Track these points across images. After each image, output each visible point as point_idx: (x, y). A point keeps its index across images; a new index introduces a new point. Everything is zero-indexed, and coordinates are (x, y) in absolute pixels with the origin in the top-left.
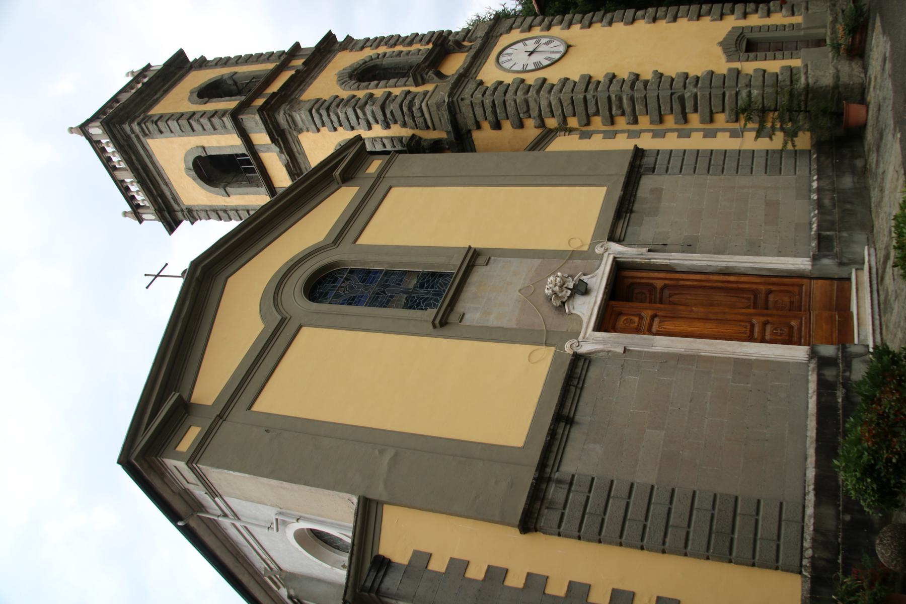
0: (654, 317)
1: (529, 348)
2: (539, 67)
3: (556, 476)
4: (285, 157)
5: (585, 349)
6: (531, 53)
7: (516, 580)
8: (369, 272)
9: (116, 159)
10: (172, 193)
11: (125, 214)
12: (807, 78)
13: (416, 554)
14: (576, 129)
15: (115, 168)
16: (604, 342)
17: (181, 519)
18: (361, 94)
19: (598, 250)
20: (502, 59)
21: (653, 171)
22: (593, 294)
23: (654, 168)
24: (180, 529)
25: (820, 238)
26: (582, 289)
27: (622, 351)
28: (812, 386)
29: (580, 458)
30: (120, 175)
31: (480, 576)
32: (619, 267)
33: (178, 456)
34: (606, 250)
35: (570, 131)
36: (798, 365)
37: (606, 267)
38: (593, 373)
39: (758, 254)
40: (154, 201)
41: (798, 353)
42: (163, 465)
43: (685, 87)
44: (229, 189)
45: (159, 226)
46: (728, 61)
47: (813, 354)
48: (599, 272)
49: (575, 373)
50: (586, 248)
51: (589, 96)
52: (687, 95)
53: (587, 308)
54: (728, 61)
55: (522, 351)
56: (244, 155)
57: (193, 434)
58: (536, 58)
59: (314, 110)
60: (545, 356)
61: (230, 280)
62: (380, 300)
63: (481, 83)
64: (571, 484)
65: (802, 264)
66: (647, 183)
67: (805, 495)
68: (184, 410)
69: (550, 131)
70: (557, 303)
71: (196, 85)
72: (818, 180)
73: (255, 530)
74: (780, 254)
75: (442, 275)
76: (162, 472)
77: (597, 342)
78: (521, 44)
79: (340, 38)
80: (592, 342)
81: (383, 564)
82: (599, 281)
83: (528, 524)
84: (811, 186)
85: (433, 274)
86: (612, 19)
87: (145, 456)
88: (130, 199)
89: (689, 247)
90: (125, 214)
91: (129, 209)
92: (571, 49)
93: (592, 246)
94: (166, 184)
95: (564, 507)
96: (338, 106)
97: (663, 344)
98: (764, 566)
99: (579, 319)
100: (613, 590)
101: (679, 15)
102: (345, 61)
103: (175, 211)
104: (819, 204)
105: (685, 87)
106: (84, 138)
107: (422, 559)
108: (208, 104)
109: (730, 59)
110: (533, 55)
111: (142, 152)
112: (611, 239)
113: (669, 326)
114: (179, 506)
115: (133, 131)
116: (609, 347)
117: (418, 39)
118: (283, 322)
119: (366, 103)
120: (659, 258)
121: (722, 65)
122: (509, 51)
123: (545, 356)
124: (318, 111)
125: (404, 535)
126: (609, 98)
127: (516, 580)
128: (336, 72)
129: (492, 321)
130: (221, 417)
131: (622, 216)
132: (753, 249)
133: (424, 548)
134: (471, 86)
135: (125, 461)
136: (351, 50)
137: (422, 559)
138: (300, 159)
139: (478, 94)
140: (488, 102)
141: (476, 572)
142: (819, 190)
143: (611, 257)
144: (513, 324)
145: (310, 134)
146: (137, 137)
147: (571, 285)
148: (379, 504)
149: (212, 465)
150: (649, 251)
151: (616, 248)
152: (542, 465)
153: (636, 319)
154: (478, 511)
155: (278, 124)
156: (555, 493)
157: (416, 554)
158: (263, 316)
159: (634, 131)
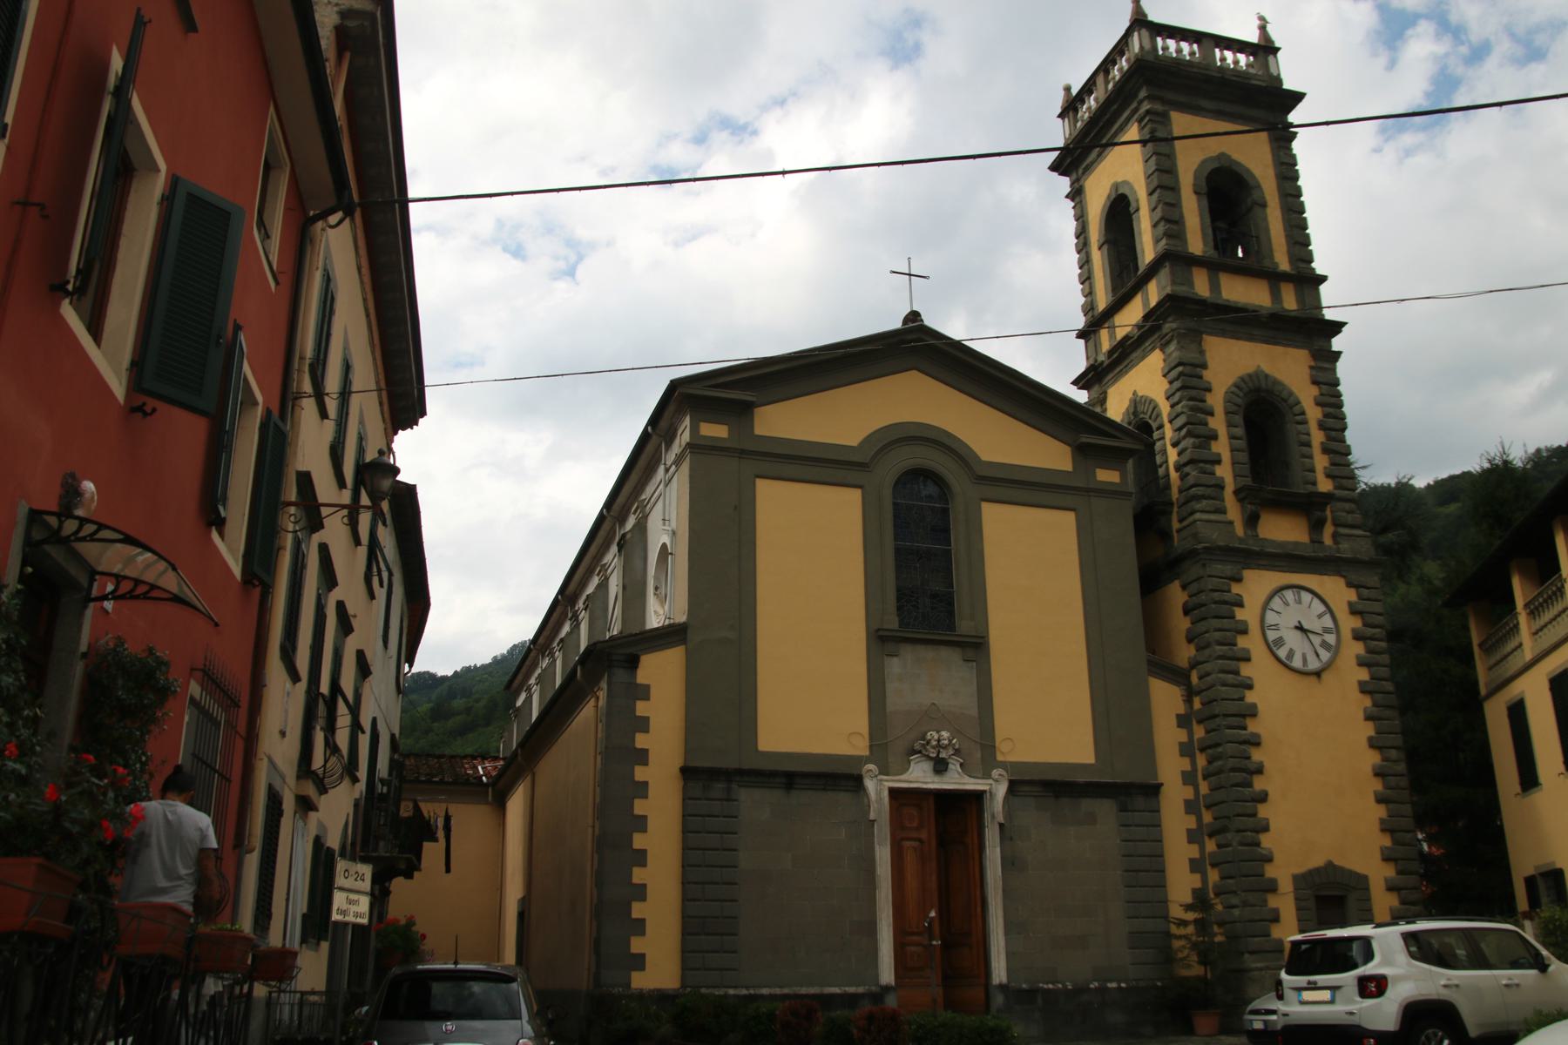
0: (920, 840)
1: (865, 730)
2: (1271, 648)
3: (734, 786)
5: (870, 784)
6: (1300, 628)
7: (640, 773)
8: (947, 531)
9: (1116, 73)
10: (1092, 163)
11: (1068, 89)
12: (1261, 969)
13: (647, 687)
14: (1191, 707)
15: (1107, 72)
16: (880, 799)
18: (1218, 423)
19: (995, 773)
20: (1289, 595)
22: (936, 779)
23: (1126, 810)
24: (645, 432)
26: (940, 767)
27: (872, 817)
28: (852, 990)
29: (755, 805)
30: (1100, 80)
32: (977, 797)
35: (1188, 700)
36: (877, 976)
37: (971, 784)
38: (843, 797)
39: (1007, 933)
41: (887, 975)
42: (684, 415)
43: (1238, 831)
48: (967, 779)
49: (840, 779)
50: (1000, 758)
52: (1229, 836)
53: (919, 776)
55: (862, 724)
57: (716, 431)
58: (1293, 640)
59: (1180, 368)
60: (860, 747)
61: (914, 372)
64: (728, 800)
65: (999, 972)
66: (1105, 809)
67: (747, 988)
68: (740, 412)
69: (1188, 677)
70: (917, 747)
72: (1120, 988)
73: (660, 503)
74: (1010, 955)
75: (951, 614)
76: (680, 413)
77: (878, 793)
78: (1322, 608)
79: (1337, 343)
80: (876, 787)
81: (633, 663)
82: (956, 780)
83: (687, 772)
84: (1111, 981)
85: (951, 604)
86: (1379, 719)
87: (687, 398)
88: (1088, 88)
90: (1068, 89)
93: (1004, 765)
96: (1191, 399)
97: (883, 855)
98: (684, 960)
99: (905, 768)
101: (1391, 806)
104: (1080, 990)
105: (1238, 831)
106: (1127, 24)
107: (644, 693)
108: (1194, 197)
109: (1301, 881)
110: (1298, 633)
112: (1012, 784)
113: (910, 859)
114: (663, 424)
115: (1141, 102)
116: (874, 806)
117: (1338, 459)
118: (862, 466)
119: (1197, 436)
120: (992, 837)
121: (1282, 871)
122: (1306, 597)
123: (860, 747)
124: (1181, 374)
125: (662, 672)
127: (640, 773)
128: (1266, 369)
129: (891, 687)
130: (743, 453)
131: (1047, 788)
133: (653, 691)
134: (1228, 569)
135: (674, 386)
136: (1311, 368)
137: (644, 693)
139: (1212, 583)
140: (1203, 597)
141: (641, 741)
142: (1103, 990)
143: (986, 788)
144: (890, 708)
145: (1161, 364)
146: (1136, 110)
148: (683, 641)
149: (691, 469)
150: (1001, 825)
152: (741, 772)
154: (693, 728)
156: (719, 788)
157: (647, 687)
158: (868, 440)
159: (1196, 776)
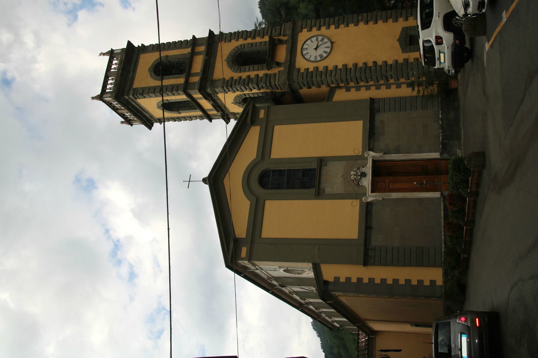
0: (389, 182)
1: (351, 201)
2: (323, 59)
4: (211, 102)
5: (370, 199)
6: (316, 49)
10: (150, 115)
11: (122, 122)
13: (335, 277)
15: (117, 109)
16: (375, 196)
17: (242, 274)
18: (244, 75)
19: (366, 155)
21: (379, 112)
22: (368, 176)
25: (443, 144)
26: (364, 175)
29: (377, 240)
30: (120, 111)
31: (356, 281)
33: (244, 259)
34: (369, 155)
35: (341, 88)
36: (437, 198)
37: (370, 164)
39: (422, 152)
40: (135, 115)
41: (437, 195)
42: (238, 263)
44: (180, 111)
45: (143, 127)
46: (403, 52)
47: (442, 195)
48: (368, 165)
49: (368, 210)
50: (360, 154)
51: (348, 78)
53: (367, 182)
54: (403, 52)
55: (348, 202)
56: (188, 101)
57: (244, 251)
58: (320, 51)
62: (290, 186)
63: (299, 69)
64: (375, 250)
65: (436, 155)
66: (378, 117)
68: (237, 242)
70: (357, 183)
71: (150, 65)
72: (442, 113)
74: (430, 151)
77: (373, 196)
78: (309, 41)
80: (371, 197)
81: (326, 283)
82: (368, 169)
83: (365, 264)
87: (232, 262)
89: (397, 151)
90: (122, 122)
91: (123, 120)
92: (334, 44)
93: (363, 152)
94: (147, 112)
95: (375, 257)
96: (235, 84)
97: (395, 195)
99: (365, 187)
100: (393, 279)
101: (378, 19)
102: (225, 50)
103: (151, 120)
104: (442, 127)
107: (337, 279)
110: (318, 49)
111: (133, 103)
120: (388, 157)
126: (357, 78)
127: (366, 281)
129: (335, 191)
130: (252, 242)
131: (371, 137)
132: (420, 151)
134: (295, 73)
137: (337, 279)
138: (218, 102)
142: (442, 119)
146: (132, 100)
147: (359, 174)
150: (384, 154)
151: (372, 153)
152: (365, 245)
153: (384, 184)
155: (207, 93)
157: (335, 277)
